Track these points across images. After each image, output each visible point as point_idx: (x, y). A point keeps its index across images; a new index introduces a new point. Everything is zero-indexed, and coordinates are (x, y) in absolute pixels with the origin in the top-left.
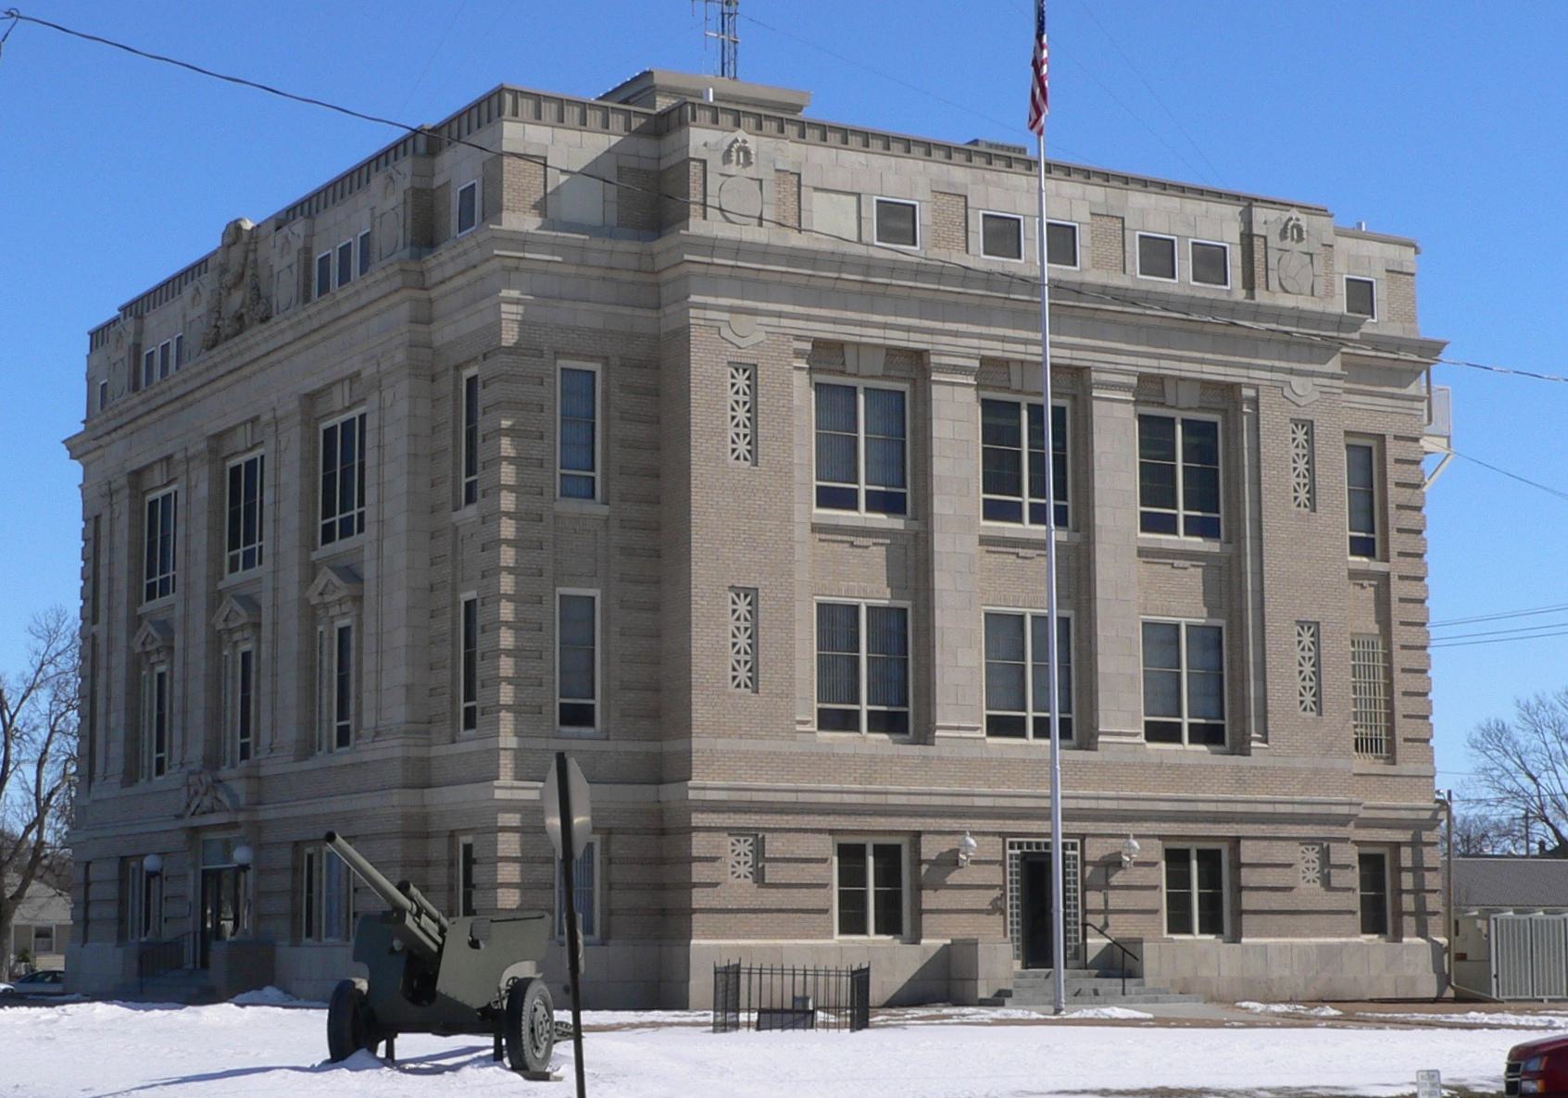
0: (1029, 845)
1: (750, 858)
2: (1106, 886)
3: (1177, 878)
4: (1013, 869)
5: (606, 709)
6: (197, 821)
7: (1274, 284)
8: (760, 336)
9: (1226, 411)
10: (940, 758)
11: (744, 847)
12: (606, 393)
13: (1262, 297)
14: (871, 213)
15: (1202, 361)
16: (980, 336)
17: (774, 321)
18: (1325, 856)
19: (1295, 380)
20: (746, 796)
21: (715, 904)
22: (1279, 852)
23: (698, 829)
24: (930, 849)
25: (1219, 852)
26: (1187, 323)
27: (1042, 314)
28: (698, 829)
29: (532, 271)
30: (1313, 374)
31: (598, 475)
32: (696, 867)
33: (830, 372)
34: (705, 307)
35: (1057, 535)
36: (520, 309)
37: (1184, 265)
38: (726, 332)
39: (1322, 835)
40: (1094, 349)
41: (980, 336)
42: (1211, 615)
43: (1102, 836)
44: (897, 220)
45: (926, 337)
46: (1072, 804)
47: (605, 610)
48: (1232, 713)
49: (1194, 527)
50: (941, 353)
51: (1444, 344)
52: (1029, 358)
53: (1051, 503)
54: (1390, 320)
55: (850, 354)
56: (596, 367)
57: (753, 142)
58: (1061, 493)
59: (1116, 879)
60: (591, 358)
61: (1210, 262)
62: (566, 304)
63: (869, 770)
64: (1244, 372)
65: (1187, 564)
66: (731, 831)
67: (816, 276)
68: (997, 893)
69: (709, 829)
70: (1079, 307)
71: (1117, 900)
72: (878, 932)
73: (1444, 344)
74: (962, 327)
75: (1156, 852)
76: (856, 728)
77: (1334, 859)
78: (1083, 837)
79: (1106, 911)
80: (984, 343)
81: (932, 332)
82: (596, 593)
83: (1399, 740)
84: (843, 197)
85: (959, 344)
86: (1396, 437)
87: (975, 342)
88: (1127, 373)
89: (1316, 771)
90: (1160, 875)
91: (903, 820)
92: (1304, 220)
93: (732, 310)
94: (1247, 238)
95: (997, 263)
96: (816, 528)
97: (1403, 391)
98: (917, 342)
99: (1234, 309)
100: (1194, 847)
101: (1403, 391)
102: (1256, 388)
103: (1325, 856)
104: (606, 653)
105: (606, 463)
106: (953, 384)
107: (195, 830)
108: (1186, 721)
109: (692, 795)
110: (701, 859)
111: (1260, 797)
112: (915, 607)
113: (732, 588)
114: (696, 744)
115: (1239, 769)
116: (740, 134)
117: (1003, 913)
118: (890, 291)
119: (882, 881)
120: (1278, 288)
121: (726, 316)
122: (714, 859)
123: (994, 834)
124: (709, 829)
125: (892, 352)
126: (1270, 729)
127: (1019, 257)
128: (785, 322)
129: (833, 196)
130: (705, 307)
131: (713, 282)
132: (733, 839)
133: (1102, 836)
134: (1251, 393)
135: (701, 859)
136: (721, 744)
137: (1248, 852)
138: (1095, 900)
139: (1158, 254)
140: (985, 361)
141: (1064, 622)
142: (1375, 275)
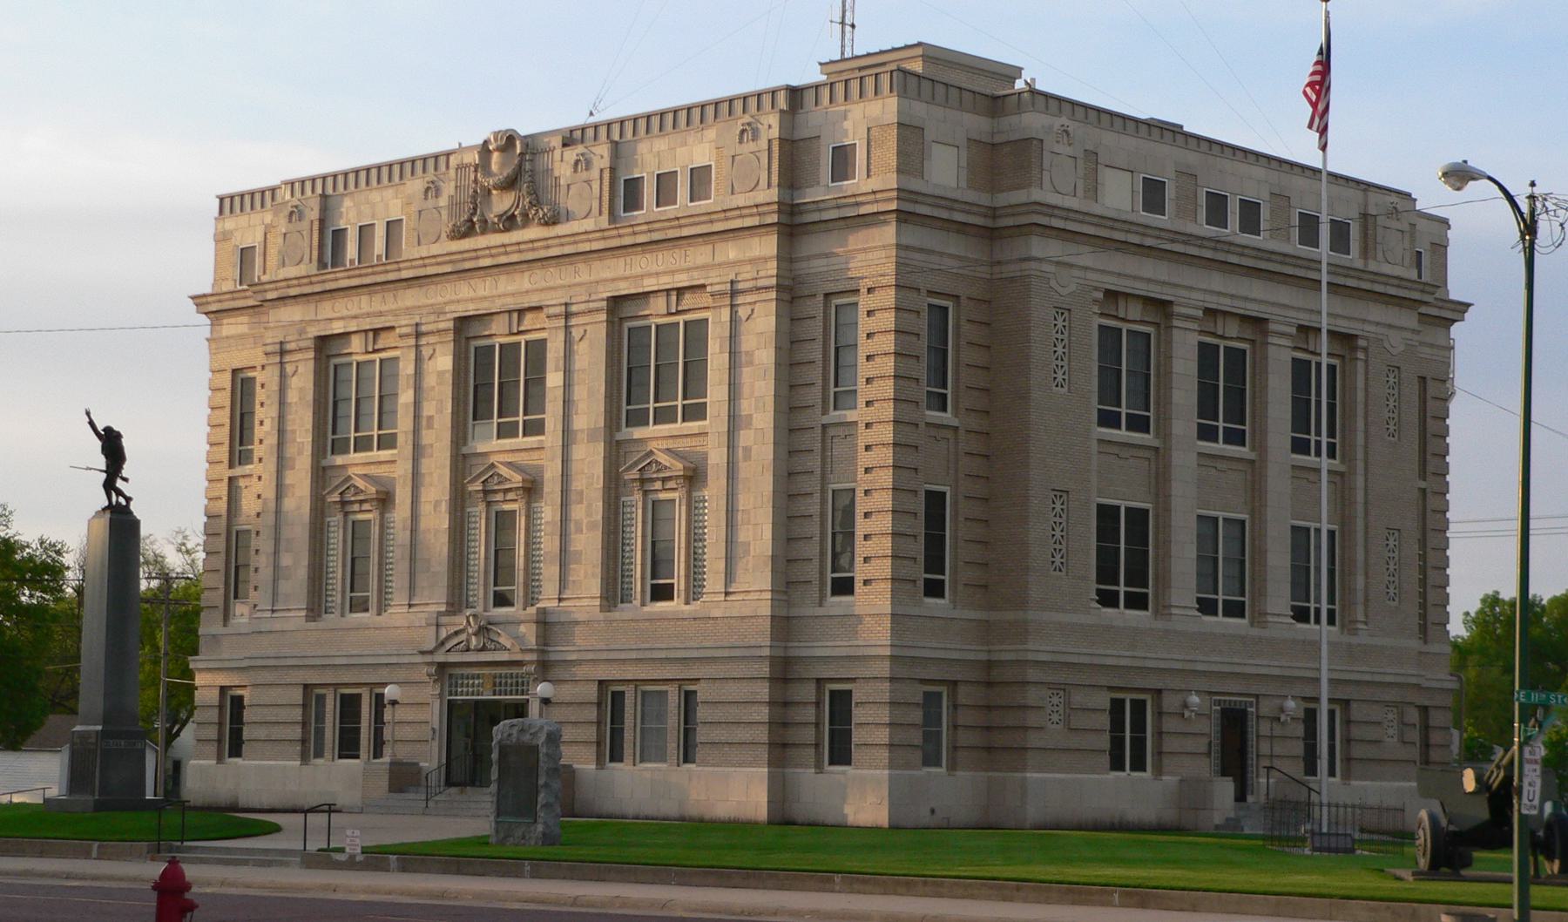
4: (1216, 718)
5: (954, 582)
6: (454, 658)
7: (1380, 255)
9: (1253, 341)
12: (957, 326)
13: (1373, 266)
18: (1402, 714)
19: (1391, 333)
24: (1266, 708)
25: (359, 696)
35: (1325, 462)
38: (1053, 283)
47: (955, 503)
48: (1342, 599)
50: (1278, 322)
51: (1469, 305)
53: (1324, 440)
56: (949, 304)
57: (1073, 127)
58: (1331, 434)
63: (1128, 640)
67: (1110, 237)
73: (1469, 305)
75: (1103, 700)
76: (1117, 606)
78: (1257, 696)
82: (947, 489)
88: (1289, 324)
90: (1104, 721)
95: (1213, 231)
96: (1100, 441)
103: (1402, 714)
104: (955, 538)
105: (957, 380)
107: (442, 666)
108: (1221, 597)
112: (1156, 508)
116: (1064, 120)
141: (1331, 534)
142: (1168, 178)
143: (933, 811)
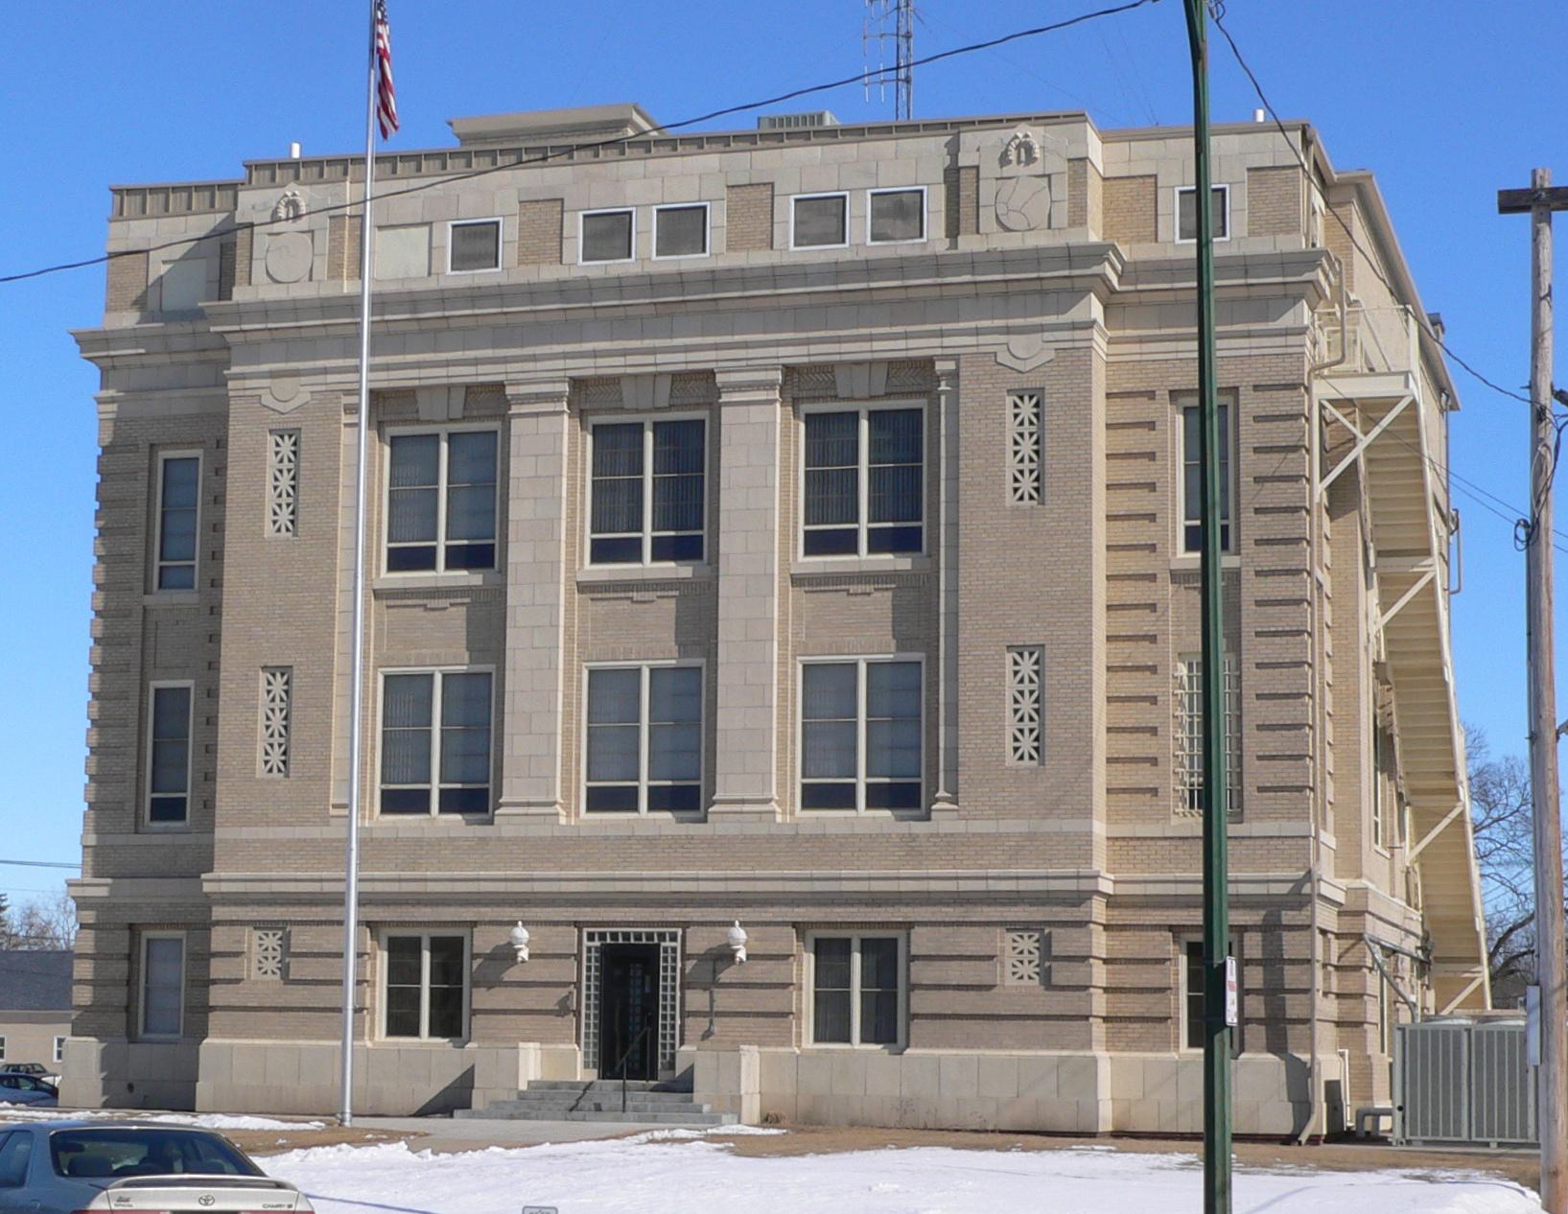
0: (614, 936)
1: (278, 954)
2: (712, 984)
3: (402, 970)
8: (305, 397)
10: (500, 839)
11: (1028, 943)
14: (446, 237)
15: (871, 338)
16: (565, 356)
17: (320, 378)
20: (264, 887)
21: (235, 1001)
22: (970, 941)
23: (218, 923)
24: (700, 942)
26: (852, 296)
27: (359, 336)
28: (218, 923)
29: (129, 367)
30: (1042, 328)
31: (157, 563)
32: (214, 963)
33: (405, 422)
34: (243, 377)
36: (114, 407)
37: (646, 232)
38: (267, 400)
39: (1039, 918)
40: (716, 347)
41: (565, 356)
42: (900, 648)
43: (713, 924)
44: (476, 242)
45: (501, 368)
46: (368, 887)
49: (880, 542)
50: (518, 383)
52: (877, 356)
54: (1251, 233)
55: (840, 376)
59: (725, 976)
60: (191, 445)
61: (899, 210)
62: (158, 395)
64: (936, 342)
65: (869, 588)
66: (258, 925)
68: (563, 992)
69: (232, 923)
70: (669, 303)
71: (725, 1000)
72: (432, 1033)
74: (539, 350)
76: (426, 810)
77: (1056, 950)
78: (685, 925)
79: (711, 1014)
80: (570, 363)
81: (505, 360)
82: (189, 683)
83: (1250, 791)
84: (413, 230)
85: (541, 369)
86: (1256, 388)
87: (560, 364)
88: (765, 368)
89: (1031, 837)
91: (452, 909)
92: (1036, 135)
93: (273, 375)
94: (953, 176)
97: (1271, 325)
98: (488, 374)
99: (936, 265)
100: (425, 935)
101: (1271, 325)
102: (956, 358)
106: (537, 415)
109: (207, 887)
110: (1292, 962)
111: (938, 875)
113: (265, 668)
114: (220, 833)
115: (913, 837)
117: (577, 1013)
118: (452, 323)
119: (439, 979)
120: (995, 226)
121: (265, 382)
122: (237, 954)
123: (568, 923)
124: (232, 923)
125: (894, 365)
126: (962, 786)
127: (704, 250)
128: (331, 378)
129: (402, 231)
130: (243, 377)
131: (254, 350)
132: (259, 933)
133: (713, 924)
134: (951, 366)
135: (1292, 962)
136: (246, 833)
137: (922, 941)
138: (697, 999)
139: (823, 216)
140: (789, 370)
143: (131, 1087)
